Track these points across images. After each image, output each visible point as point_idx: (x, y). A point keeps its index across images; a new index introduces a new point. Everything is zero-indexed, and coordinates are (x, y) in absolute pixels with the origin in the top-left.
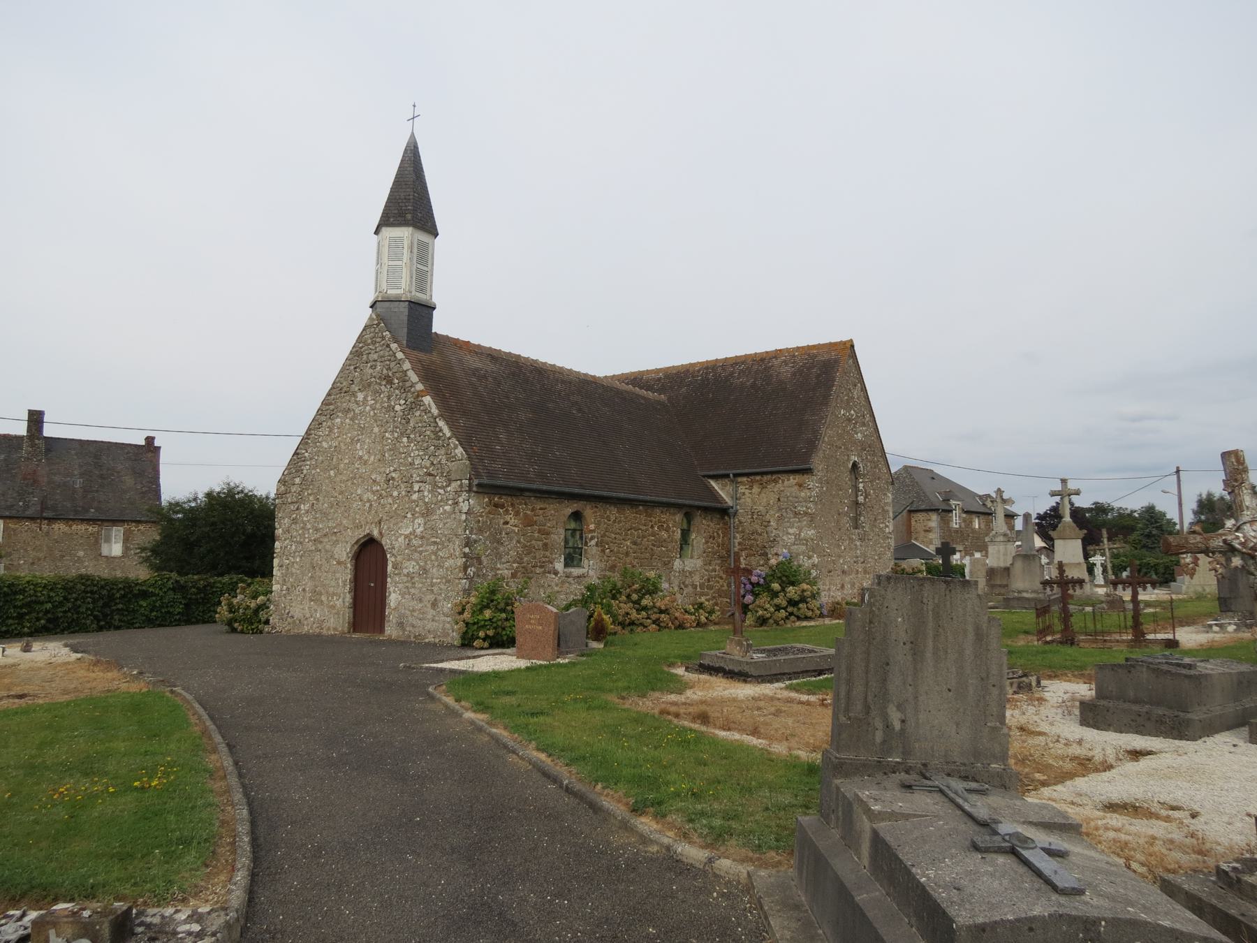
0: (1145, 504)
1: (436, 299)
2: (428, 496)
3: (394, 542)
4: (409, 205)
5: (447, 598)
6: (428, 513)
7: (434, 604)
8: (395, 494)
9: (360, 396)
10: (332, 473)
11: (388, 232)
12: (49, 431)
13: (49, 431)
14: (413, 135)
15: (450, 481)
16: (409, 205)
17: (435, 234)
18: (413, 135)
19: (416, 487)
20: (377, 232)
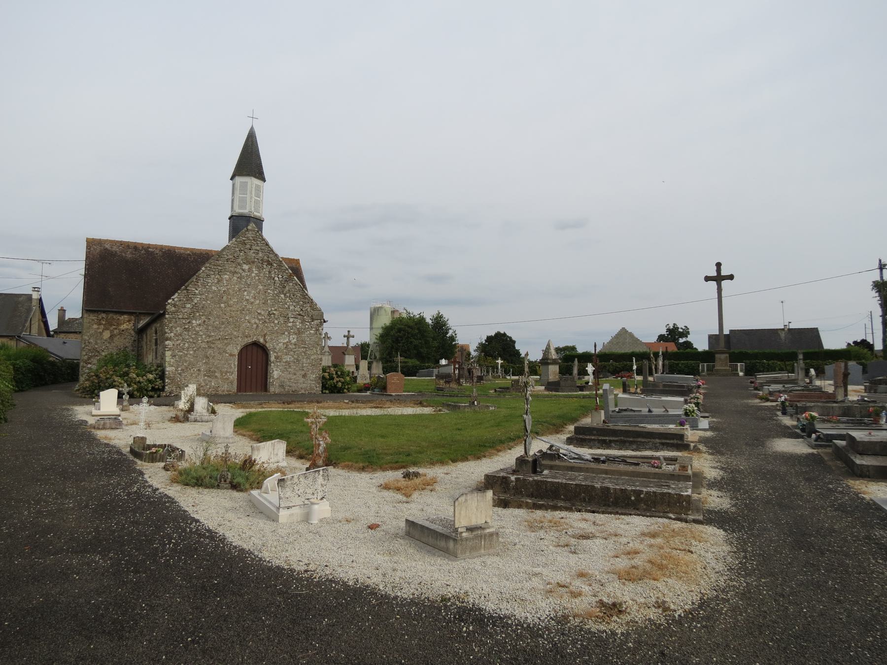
0: (616, 330)
1: (265, 213)
2: (299, 325)
3: (277, 345)
4: (249, 164)
5: (313, 373)
6: (299, 332)
7: (304, 376)
8: (276, 322)
9: (246, 267)
10: (222, 305)
11: (238, 179)
12: (68, 316)
13: (68, 316)
14: (252, 128)
15: (313, 320)
16: (249, 164)
17: (264, 180)
18: (252, 128)
19: (291, 320)
20: (232, 179)
